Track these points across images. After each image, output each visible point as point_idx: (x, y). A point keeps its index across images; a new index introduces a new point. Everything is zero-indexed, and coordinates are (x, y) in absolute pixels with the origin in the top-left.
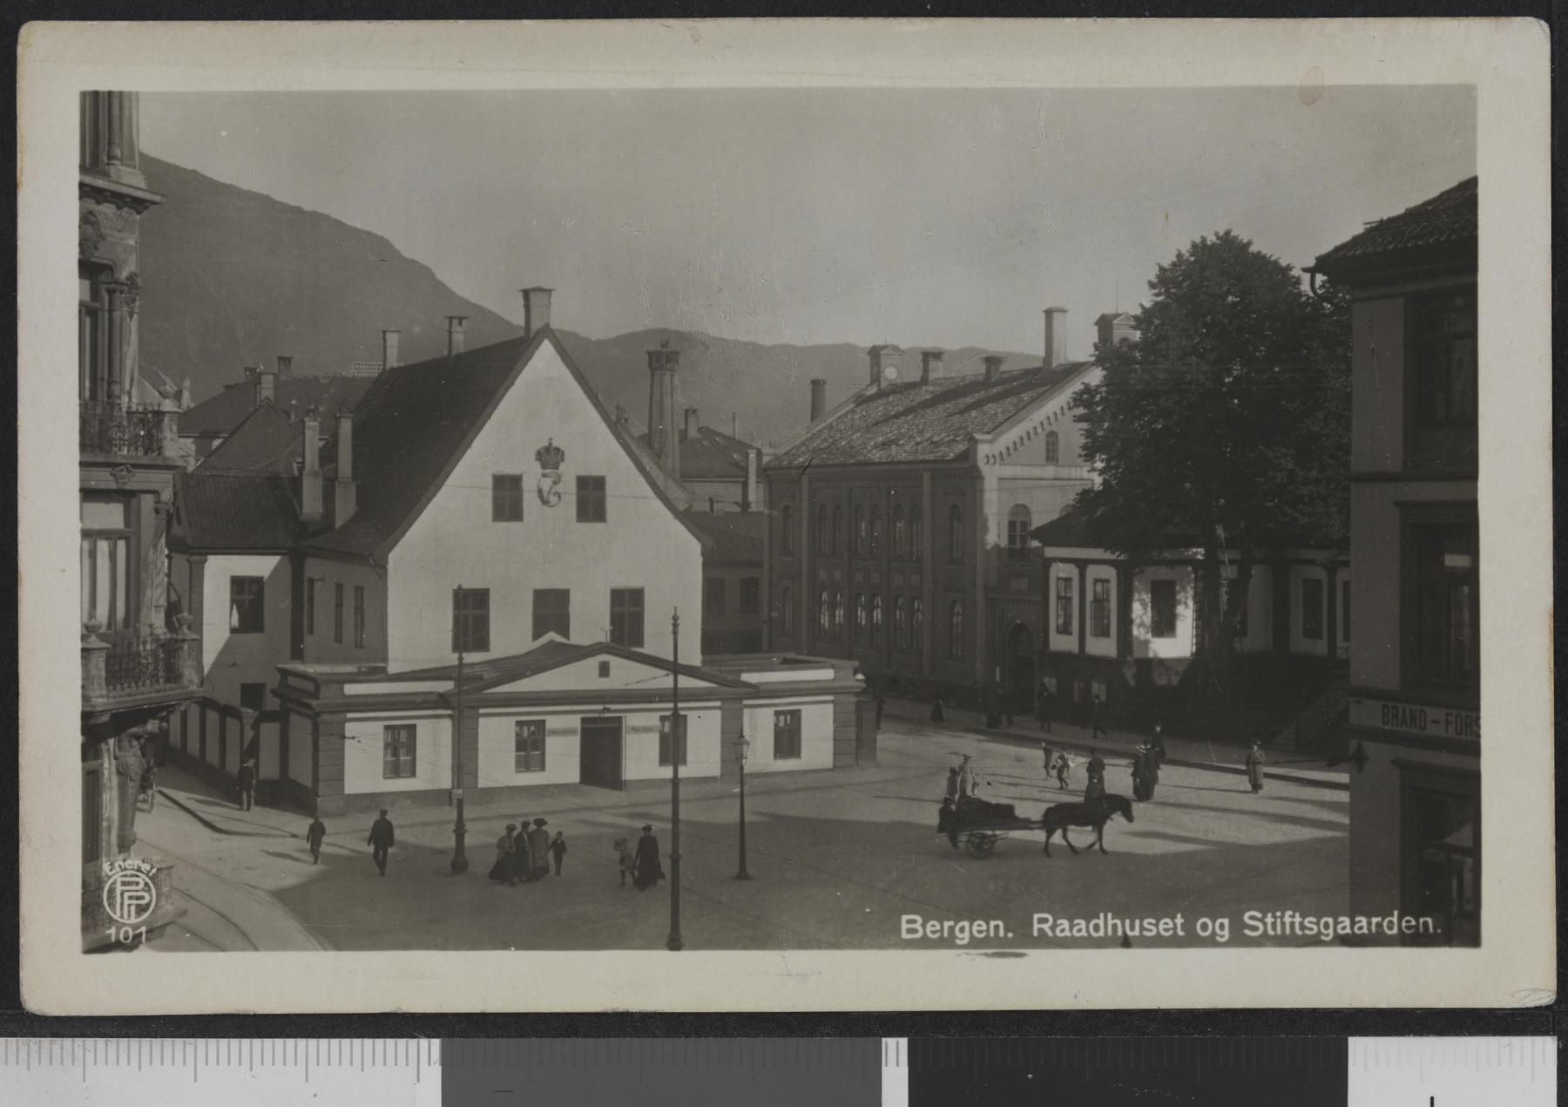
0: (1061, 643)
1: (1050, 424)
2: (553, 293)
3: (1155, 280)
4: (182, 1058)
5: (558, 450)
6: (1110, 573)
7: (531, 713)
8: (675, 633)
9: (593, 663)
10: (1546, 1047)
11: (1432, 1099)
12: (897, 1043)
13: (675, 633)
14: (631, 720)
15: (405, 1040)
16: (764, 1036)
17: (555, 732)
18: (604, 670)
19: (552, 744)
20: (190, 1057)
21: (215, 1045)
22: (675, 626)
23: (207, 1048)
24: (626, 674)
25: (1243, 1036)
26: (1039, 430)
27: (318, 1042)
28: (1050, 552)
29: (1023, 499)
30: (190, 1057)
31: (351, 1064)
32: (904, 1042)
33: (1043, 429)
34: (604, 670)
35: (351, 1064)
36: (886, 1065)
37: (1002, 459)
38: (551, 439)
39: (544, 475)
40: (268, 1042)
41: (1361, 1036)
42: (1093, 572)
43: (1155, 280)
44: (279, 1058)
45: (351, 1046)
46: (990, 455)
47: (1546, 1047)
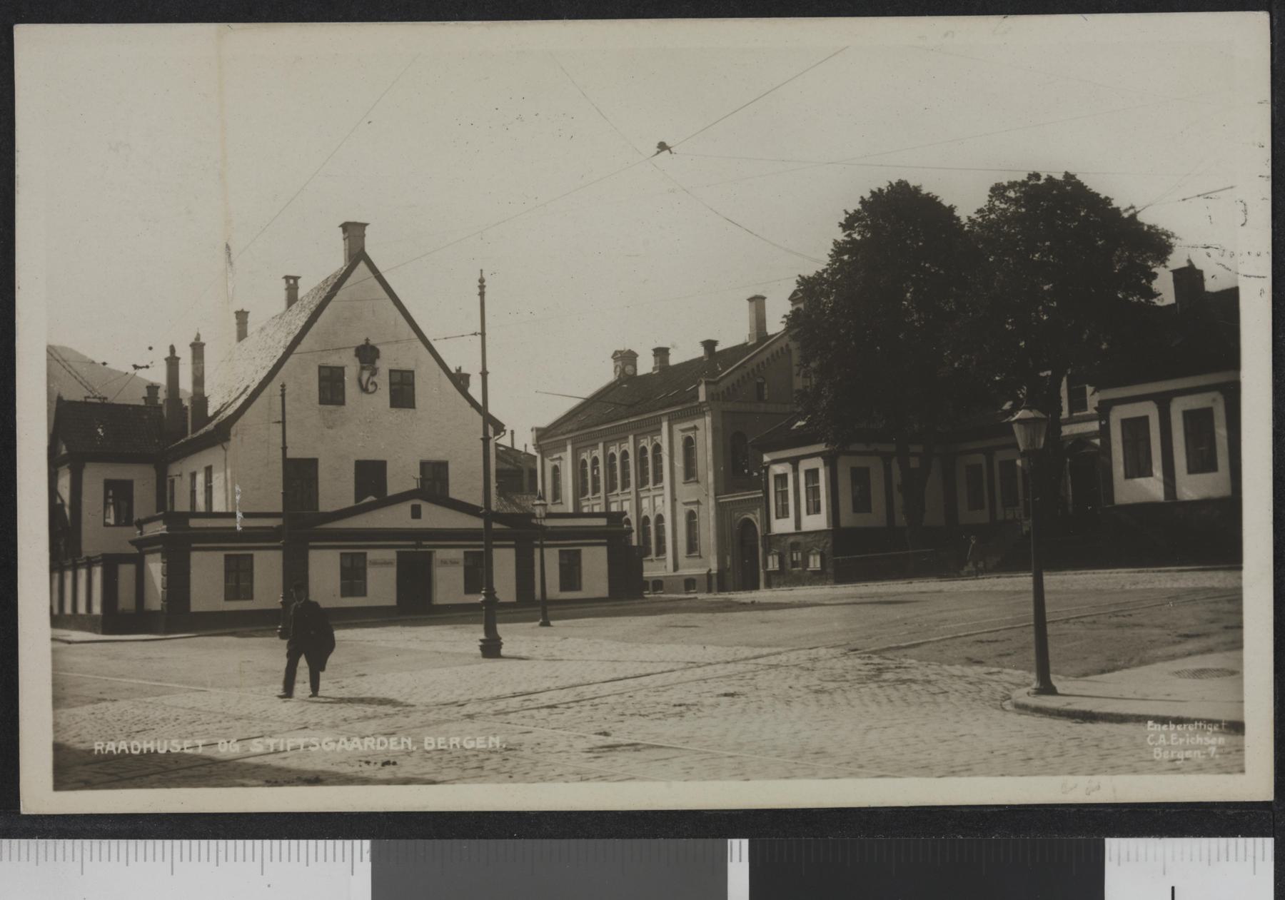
0: (781, 526)
3: (843, 222)
4: (161, 856)
6: (818, 463)
8: (482, 294)
9: (406, 508)
11: (1173, 888)
12: (740, 843)
13: (482, 294)
14: (440, 554)
15: (117, 840)
17: (375, 563)
18: (416, 513)
19: (372, 573)
20: (78, 854)
21: (125, 846)
22: (482, 287)
23: (109, 847)
24: (435, 517)
25: (804, 838)
27: (100, 843)
30: (78, 854)
32: (745, 842)
34: (416, 513)
35: (298, 860)
36: (731, 861)
40: (177, 842)
41: (1169, 837)
43: (843, 222)
44: (195, 855)
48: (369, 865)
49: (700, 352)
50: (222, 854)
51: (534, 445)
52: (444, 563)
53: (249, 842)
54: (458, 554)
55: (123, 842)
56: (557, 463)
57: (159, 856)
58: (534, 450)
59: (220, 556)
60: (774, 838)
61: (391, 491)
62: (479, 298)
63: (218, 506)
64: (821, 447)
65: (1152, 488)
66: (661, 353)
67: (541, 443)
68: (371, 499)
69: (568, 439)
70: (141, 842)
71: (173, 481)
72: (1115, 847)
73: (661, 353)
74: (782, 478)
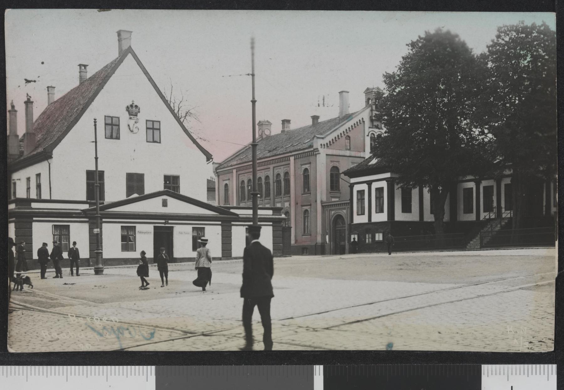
0: (359, 219)
1: (347, 133)
2: (132, 33)
5: (136, 106)
7: (129, 222)
9: (159, 200)
10: (553, 368)
11: (512, 387)
12: (528, 367)
13: (95, 125)
16: (224, 365)
18: (165, 204)
26: (343, 135)
28: (353, 180)
29: (336, 164)
31: (123, 375)
32: (322, 367)
33: (344, 135)
34: (165, 204)
35: (123, 375)
36: (315, 375)
37: (328, 147)
38: (133, 101)
39: (130, 118)
42: (375, 186)
44: (17, 372)
45: (31, 369)
46: (323, 144)
47: (553, 368)
48: (155, 377)
49: (310, 122)
50: (89, 372)
51: (214, 172)
52: (181, 233)
53: (101, 367)
54: (189, 228)
55: (45, 367)
56: (227, 182)
57: (41, 373)
58: (214, 175)
59: (51, 224)
60: (370, 365)
61: (147, 191)
62: (94, 126)
63: (46, 196)
64: (388, 175)
65: (472, 217)
66: (286, 122)
67: (218, 171)
68: (135, 195)
69: (235, 168)
70: (53, 367)
71: (15, 184)
72: (485, 368)
73: (286, 122)
74: (361, 193)
